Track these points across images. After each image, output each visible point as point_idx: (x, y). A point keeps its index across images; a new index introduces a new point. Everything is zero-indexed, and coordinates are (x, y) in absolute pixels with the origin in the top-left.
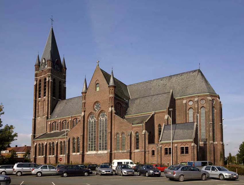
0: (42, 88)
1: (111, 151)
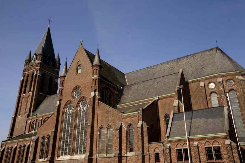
0: (29, 83)
1: (91, 154)
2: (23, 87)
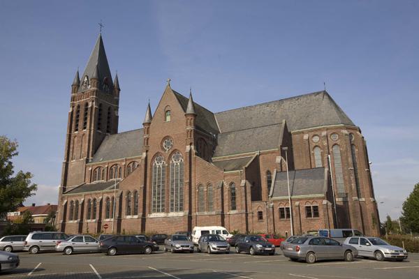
1: (190, 212)
2: (74, 122)
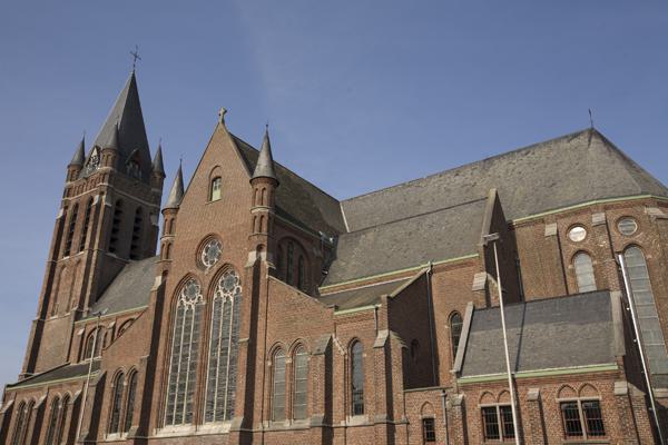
1: (248, 422)
2: (64, 238)
